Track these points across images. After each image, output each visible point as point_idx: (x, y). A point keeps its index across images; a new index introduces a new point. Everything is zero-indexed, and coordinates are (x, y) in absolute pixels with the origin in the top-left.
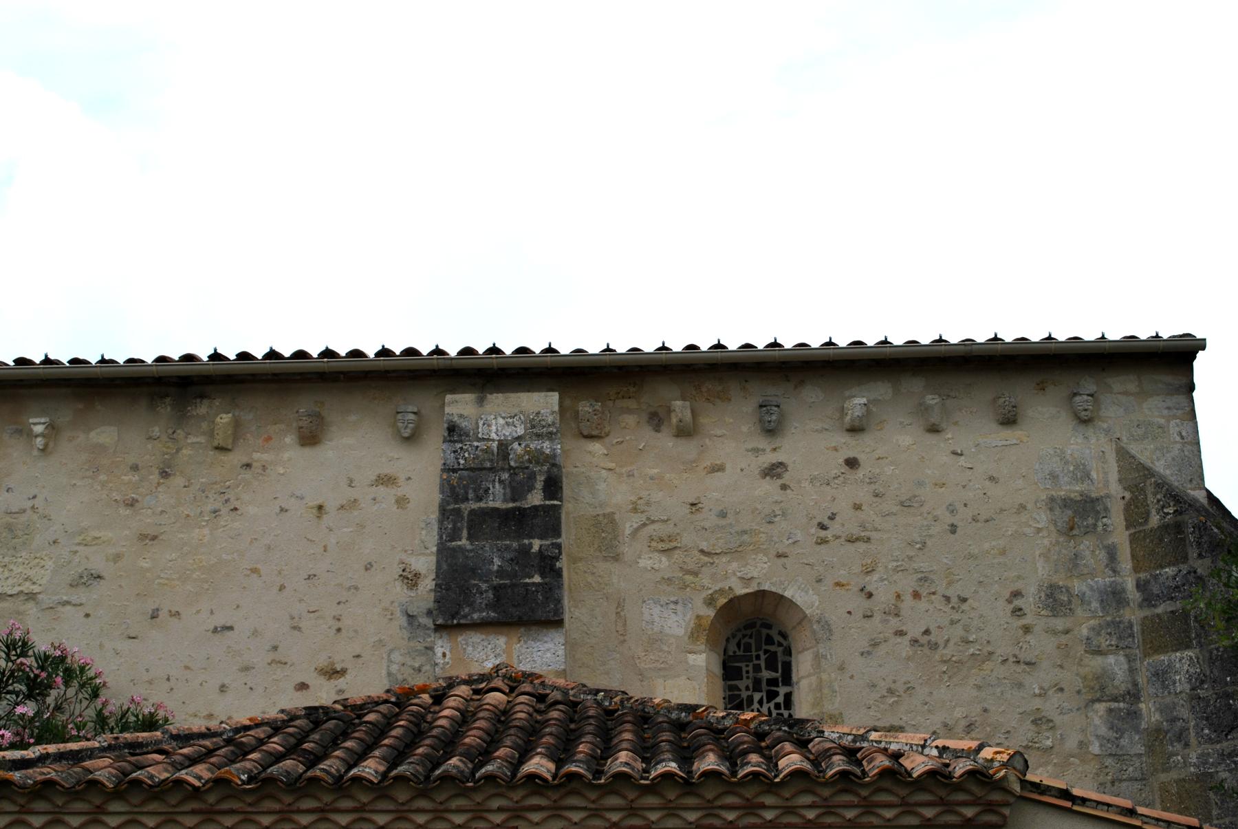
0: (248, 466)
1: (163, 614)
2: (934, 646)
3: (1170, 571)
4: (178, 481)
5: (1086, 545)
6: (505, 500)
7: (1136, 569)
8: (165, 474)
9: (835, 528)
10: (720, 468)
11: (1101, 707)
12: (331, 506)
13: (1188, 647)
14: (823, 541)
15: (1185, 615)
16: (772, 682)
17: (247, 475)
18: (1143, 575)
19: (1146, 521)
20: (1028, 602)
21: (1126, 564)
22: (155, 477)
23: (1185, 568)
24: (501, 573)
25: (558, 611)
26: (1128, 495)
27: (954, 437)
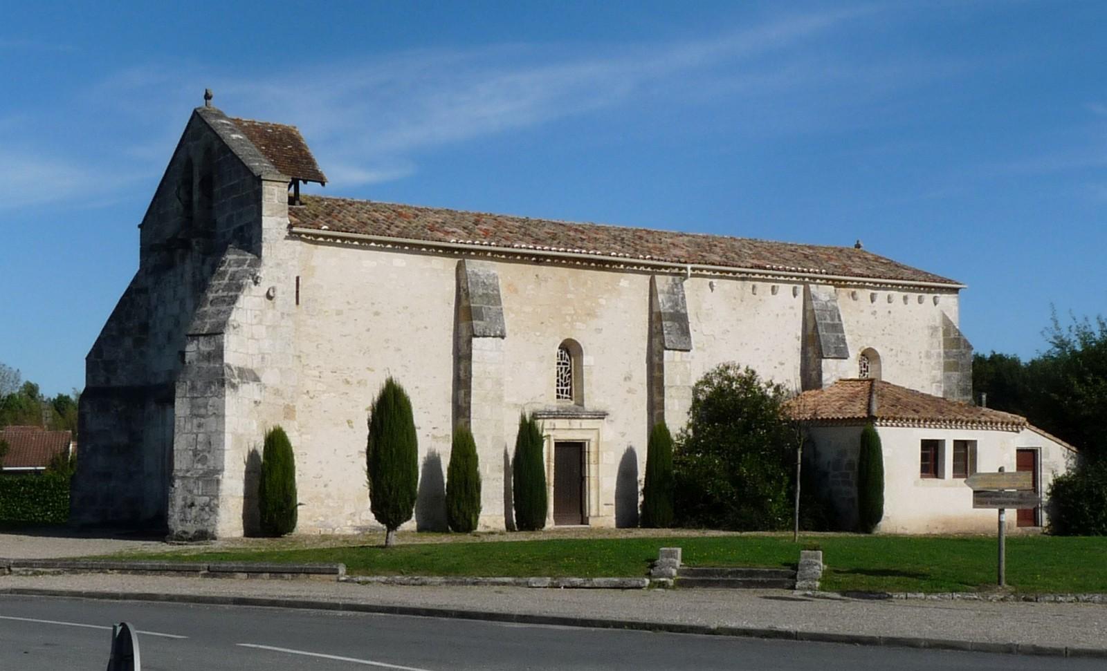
0: (760, 300)
1: (744, 344)
2: (903, 365)
3: (955, 350)
4: (745, 303)
5: (935, 340)
6: (778, 287)
7: (944, 348)
8: (742, 301)
9: (886, 331)
10: (862, 311)
11: (935, 384)
12: (780, 315)
13: (958, 371)
14: (883, 334)
15: (958, 364)
16: (865, 371)
17: (760, 303)
18: (947, 350)
19: (950, 335)
20: (923, 355)
21: (942, 347)
22: (739, 301)
23: (958, 350)
24: (835, 343)
25: (923, 448)
26: (945, 327)
27: (982, 353)
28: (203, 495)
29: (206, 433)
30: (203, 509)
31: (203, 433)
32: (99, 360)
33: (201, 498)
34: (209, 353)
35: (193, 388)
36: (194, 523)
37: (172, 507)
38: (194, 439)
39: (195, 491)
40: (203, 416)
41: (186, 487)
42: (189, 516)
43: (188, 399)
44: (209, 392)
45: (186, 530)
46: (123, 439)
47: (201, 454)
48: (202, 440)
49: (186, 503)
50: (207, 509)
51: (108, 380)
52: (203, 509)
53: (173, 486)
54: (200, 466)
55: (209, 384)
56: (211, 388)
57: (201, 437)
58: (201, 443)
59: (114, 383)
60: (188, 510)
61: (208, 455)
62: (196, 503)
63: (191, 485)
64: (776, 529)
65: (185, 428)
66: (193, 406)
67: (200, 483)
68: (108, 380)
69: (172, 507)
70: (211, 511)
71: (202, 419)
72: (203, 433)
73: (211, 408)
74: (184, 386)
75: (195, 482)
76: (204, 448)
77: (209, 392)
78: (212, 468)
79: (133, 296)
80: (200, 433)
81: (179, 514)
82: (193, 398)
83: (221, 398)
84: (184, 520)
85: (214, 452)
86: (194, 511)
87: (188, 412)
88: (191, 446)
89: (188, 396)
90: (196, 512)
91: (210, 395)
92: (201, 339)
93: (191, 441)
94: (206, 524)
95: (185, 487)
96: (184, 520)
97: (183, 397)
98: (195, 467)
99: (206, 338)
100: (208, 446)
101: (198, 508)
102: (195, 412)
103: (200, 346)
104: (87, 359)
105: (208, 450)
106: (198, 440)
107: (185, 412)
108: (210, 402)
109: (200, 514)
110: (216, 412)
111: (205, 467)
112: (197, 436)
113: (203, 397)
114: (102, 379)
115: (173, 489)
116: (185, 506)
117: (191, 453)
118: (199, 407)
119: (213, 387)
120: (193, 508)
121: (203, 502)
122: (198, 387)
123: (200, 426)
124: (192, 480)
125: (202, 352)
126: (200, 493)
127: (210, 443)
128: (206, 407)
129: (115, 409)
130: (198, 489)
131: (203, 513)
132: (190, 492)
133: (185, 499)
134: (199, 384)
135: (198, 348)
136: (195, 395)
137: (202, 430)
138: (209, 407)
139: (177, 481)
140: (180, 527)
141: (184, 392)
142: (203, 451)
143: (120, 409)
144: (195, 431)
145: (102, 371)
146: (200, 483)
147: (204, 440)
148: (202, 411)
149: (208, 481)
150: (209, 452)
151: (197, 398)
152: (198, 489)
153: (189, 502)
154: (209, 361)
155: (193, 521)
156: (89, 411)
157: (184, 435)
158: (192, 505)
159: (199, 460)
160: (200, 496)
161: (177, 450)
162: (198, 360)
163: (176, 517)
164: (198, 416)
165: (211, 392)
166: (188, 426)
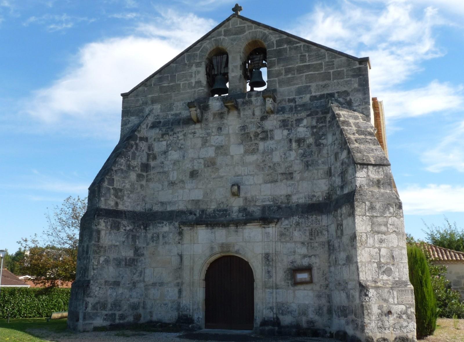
28: (398, 304)
29: (388, 248)
30: (400, 317)
31: (384, 247)
32: (111, 187)
33: (397, 306)
34: (379, 181)
35: (372, 208)
36: (393, 330)
37: (368, 315)
38: (376, 253)
39: (391, 300)
40: (384, 233)
41: (381, 296)
42: (387, 324)
43: (368, 217)
44: (388, 213)
45: (386, 337)
46: (130, 254)
47: (386, 267)
48: (384, 254)
49: (382, 312)
50: (404, 316)
51: (117, 204)
52: (400, 317)
53: (367, 295)
54: (385, 277)
55: (387, 206)
56: (389, 209)
57: (384, 252)
58: (384, 256)
59: (121, 207)
60: (385, 318)
61: (392, 267)
62: (393, 311)
63: (386, 295)
64: (462, 318)
65: (366, 243)
66: (373, 224)
67: (395, 293)
68: (117, 204)
69: (368, 315)
70: (409, 318)
71: (383, 235)
72: (384, 247)
73: (391, 227)
74: (364, 206)
75: (389, 292)
76: (389, 261)
77: (388, 213)
78: (397, 279)
79: (138, 141)
80: (382, 247)
81: (376, 322)
82: (373, 216)
83: (399, 218)
84: (382, 328)
85: (398, 264)
86: (392, 320)
87: (369, 229)
88: (375, 259)
89: (367, 214)
90: (394, 319)
91: (389, 215)
92: (370, 168)
93: (375, 254)
94: (405, 331)
95: (380, 296)
96: (382, 328)
97: (363, 216)
98: (380, 278)
99: (375, 168)
100: (392, 259)
101: (395, 316)
102: (376, 229)
103: (370, 173)
104: (89, 189)
105: (392, 263)
106: (381, 253)
107: (366, 229)
108: (390, 221)
109: (398, 323)
110: (396, 230)
111: (390, 278)
112: (380, 250)
113: (381, 216)
114: (112, 203)
115: (367, 298)
116: (381, 314)
117: (375, 265)
118: (380, 225)
119: (391, 208)
120: (390, 316)
121: (400, 310)
122: (377, 207)
123: (381, 241)
124: (386, 290)
125: (372, 179)
126: (396, 302)
127: (393, 257)
128: (386, 225)
129: (124, 228)
130: (393, 298)
131: (401, 321)
132: (386, 301)
133: (380, 308)
134: (378, 205)
135: (368, 176)
136: (375, 214)
137: (384, 245)
138: (389, 225)
139: (371, 290)
140: (378, 334)
141: (363, 210)
142: (387, 263)
143: (128, 228)
144: (377, 246)
145: (112, 196)
146: (395, 293)
147: (387, 254)
148: (383, 229)
149: (402, 291)
150: (393, 265)
151: (376, 217)
152: (393, 298)
153: (385, 310)
154: (379, 187)
155: (391, 329)
156: (104, 228)
157: (366, 249)
158: (390, 313)
159: (384, 272)
160: (396, 305)
161: (360, 262)
162: (368, 185)
163: (373, 324)
164: (378, 233)
165: (390, 213)
166: (370, 241)
